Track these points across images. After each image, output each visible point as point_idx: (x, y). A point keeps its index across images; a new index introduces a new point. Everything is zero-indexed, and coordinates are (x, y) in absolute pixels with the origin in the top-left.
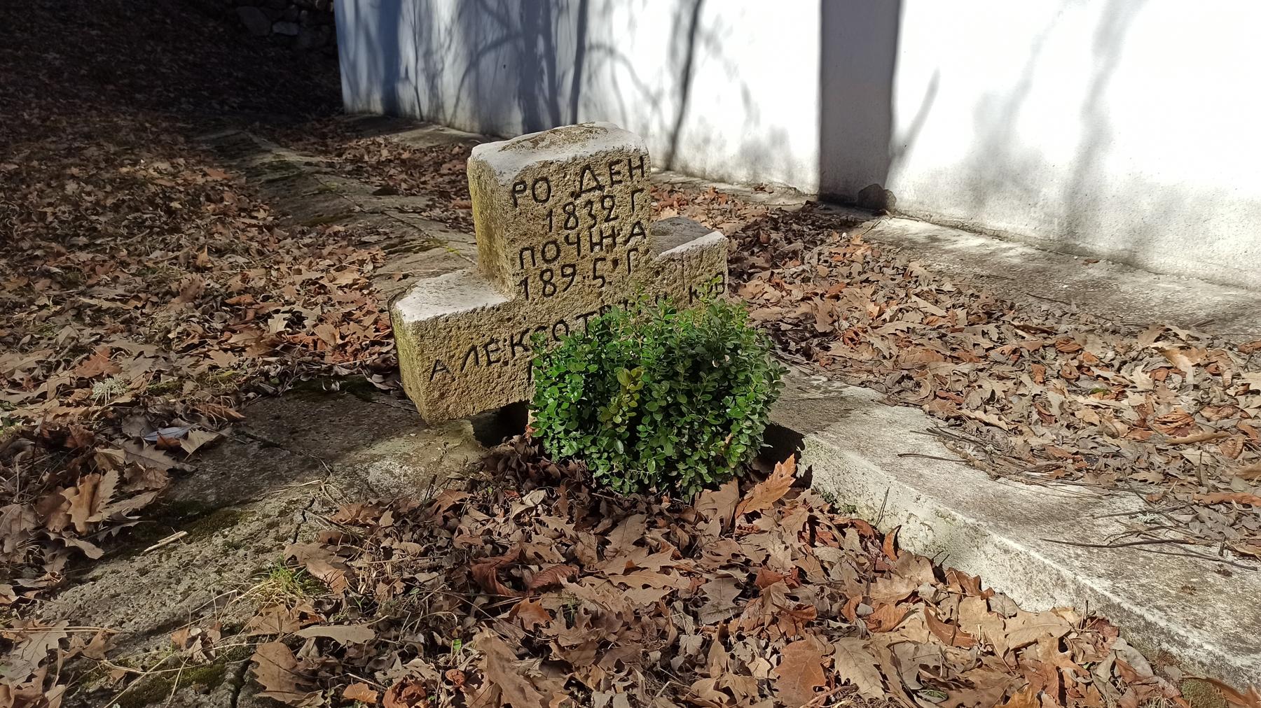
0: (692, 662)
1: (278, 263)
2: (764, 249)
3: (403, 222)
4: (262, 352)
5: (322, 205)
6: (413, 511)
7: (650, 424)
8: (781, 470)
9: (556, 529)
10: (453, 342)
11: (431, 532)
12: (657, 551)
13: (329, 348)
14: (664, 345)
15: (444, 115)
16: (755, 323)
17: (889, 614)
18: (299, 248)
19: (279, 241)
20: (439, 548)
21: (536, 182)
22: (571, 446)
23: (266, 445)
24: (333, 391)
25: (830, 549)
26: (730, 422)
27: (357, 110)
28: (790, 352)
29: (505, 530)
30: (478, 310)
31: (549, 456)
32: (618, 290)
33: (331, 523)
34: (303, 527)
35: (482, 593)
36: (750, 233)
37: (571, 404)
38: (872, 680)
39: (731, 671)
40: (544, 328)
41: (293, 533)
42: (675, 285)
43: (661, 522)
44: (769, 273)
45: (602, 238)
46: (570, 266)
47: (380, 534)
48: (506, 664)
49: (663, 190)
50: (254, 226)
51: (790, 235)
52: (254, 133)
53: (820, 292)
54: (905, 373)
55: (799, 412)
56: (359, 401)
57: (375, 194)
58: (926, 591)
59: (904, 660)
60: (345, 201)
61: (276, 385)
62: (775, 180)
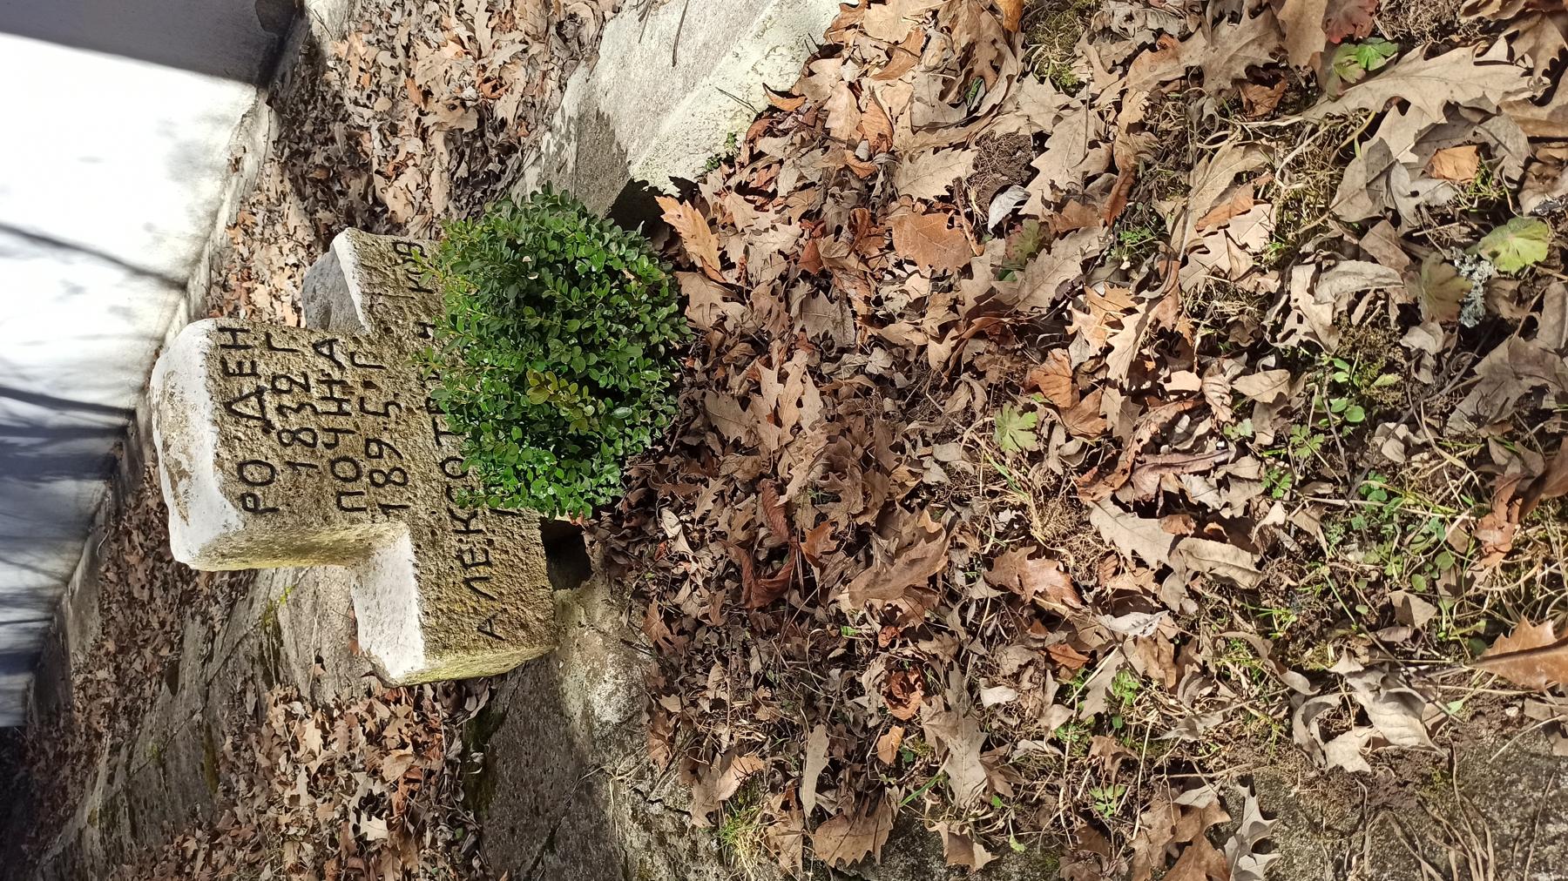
0: (901, 364)
1: (277, 825)
2: (337, 177)
3: (229, 658)
4: (414, 849)
5: (183, 765)
6: (663, 670)
7: (601, 371)
8: (672, 216)
9: (714, 501)
10: (456, 607)
11: (698, 651)
12: (758, 383)
13: (417, 763)
14: (497, 338)
15: (46, 588)
16: (452, 209)
17: (874, 125)
18: (254, 797)
19: (237, 822)
20: (720, 642)
21: (243, 479)
22: (609, 472)
23: (551, 846)
24: (484, 761)
25: (781, 176)
26: (608, 269)
27: (20, 710)
28: (503, 172)
29: (708, 562)
30: (418, 572)
31: (616, 499)
32: (405, 387)
33: (667, 769)
34: (670, 803)
35: (786, 597)
36: (308, 191)
37: (559, 465)
38: (952, 160)
39: (919, 321)
40: (449, 489)
41: (676, 816)
42: (406, 310)
43: (720, 374)
44: (377, 178)
45: (332, 398)
46: (367, 446)
47: (692, 711)
48: (882, 577)
49: (221, 297)
50: (208, 856)
51: (320, 137)
52: (42, 851)
53: (416, 115)
54: (553, 30)
55: (594, 178)
56: (503, 729)
57: (174, 690)
58: (850, 72)
59: (931, 118)
60: (182, 732)
61: (466, 832)
62: (224, 144)
